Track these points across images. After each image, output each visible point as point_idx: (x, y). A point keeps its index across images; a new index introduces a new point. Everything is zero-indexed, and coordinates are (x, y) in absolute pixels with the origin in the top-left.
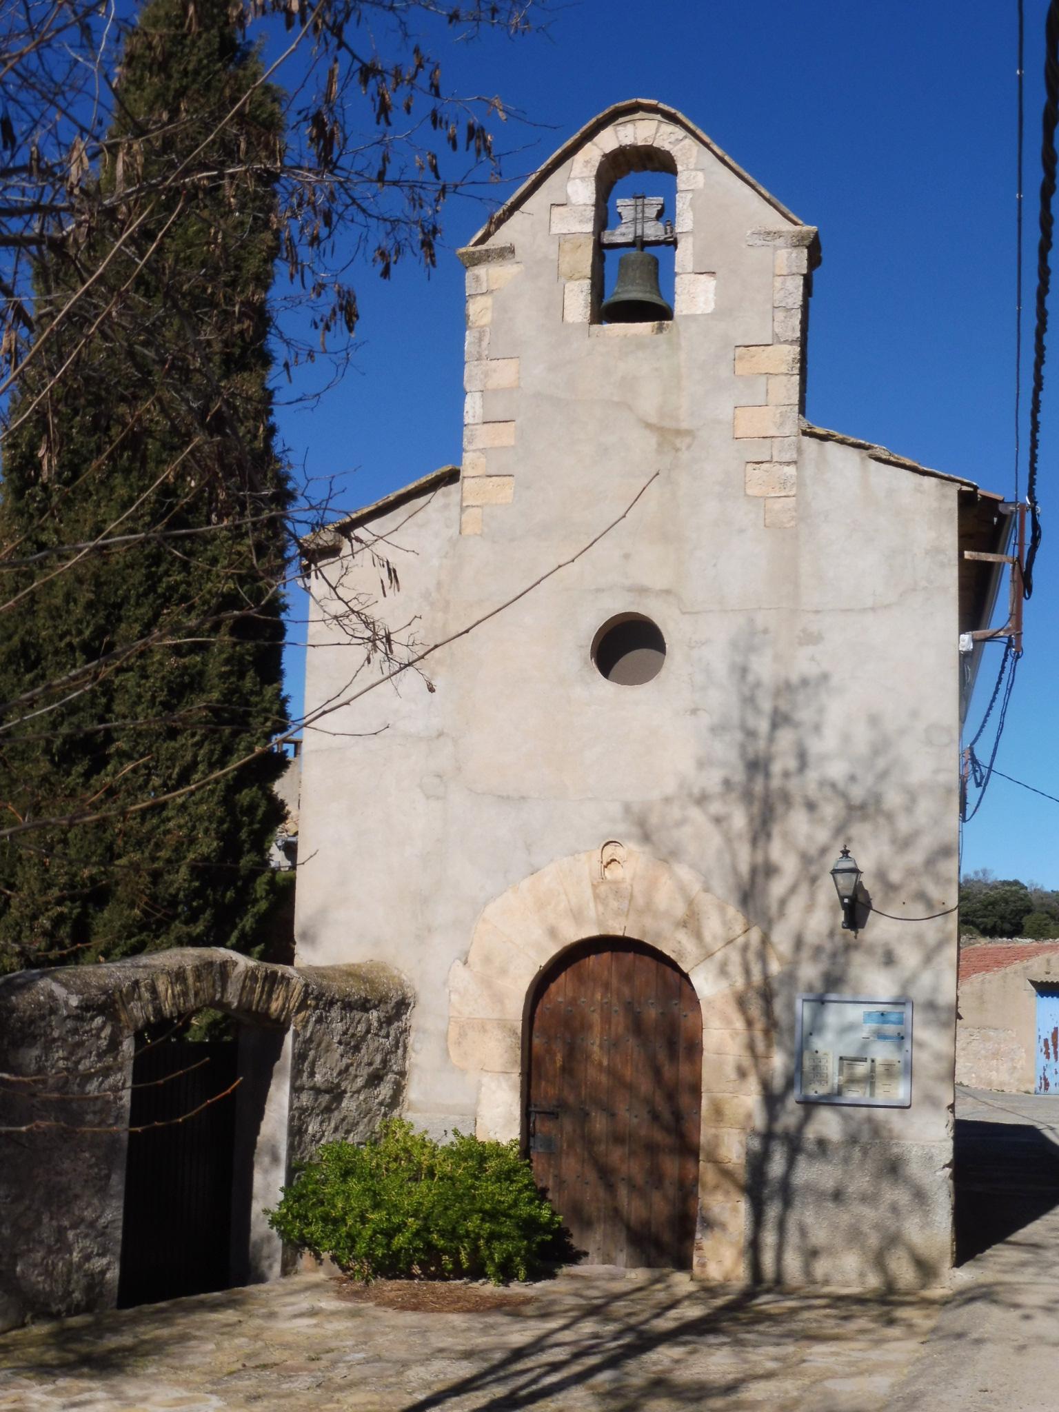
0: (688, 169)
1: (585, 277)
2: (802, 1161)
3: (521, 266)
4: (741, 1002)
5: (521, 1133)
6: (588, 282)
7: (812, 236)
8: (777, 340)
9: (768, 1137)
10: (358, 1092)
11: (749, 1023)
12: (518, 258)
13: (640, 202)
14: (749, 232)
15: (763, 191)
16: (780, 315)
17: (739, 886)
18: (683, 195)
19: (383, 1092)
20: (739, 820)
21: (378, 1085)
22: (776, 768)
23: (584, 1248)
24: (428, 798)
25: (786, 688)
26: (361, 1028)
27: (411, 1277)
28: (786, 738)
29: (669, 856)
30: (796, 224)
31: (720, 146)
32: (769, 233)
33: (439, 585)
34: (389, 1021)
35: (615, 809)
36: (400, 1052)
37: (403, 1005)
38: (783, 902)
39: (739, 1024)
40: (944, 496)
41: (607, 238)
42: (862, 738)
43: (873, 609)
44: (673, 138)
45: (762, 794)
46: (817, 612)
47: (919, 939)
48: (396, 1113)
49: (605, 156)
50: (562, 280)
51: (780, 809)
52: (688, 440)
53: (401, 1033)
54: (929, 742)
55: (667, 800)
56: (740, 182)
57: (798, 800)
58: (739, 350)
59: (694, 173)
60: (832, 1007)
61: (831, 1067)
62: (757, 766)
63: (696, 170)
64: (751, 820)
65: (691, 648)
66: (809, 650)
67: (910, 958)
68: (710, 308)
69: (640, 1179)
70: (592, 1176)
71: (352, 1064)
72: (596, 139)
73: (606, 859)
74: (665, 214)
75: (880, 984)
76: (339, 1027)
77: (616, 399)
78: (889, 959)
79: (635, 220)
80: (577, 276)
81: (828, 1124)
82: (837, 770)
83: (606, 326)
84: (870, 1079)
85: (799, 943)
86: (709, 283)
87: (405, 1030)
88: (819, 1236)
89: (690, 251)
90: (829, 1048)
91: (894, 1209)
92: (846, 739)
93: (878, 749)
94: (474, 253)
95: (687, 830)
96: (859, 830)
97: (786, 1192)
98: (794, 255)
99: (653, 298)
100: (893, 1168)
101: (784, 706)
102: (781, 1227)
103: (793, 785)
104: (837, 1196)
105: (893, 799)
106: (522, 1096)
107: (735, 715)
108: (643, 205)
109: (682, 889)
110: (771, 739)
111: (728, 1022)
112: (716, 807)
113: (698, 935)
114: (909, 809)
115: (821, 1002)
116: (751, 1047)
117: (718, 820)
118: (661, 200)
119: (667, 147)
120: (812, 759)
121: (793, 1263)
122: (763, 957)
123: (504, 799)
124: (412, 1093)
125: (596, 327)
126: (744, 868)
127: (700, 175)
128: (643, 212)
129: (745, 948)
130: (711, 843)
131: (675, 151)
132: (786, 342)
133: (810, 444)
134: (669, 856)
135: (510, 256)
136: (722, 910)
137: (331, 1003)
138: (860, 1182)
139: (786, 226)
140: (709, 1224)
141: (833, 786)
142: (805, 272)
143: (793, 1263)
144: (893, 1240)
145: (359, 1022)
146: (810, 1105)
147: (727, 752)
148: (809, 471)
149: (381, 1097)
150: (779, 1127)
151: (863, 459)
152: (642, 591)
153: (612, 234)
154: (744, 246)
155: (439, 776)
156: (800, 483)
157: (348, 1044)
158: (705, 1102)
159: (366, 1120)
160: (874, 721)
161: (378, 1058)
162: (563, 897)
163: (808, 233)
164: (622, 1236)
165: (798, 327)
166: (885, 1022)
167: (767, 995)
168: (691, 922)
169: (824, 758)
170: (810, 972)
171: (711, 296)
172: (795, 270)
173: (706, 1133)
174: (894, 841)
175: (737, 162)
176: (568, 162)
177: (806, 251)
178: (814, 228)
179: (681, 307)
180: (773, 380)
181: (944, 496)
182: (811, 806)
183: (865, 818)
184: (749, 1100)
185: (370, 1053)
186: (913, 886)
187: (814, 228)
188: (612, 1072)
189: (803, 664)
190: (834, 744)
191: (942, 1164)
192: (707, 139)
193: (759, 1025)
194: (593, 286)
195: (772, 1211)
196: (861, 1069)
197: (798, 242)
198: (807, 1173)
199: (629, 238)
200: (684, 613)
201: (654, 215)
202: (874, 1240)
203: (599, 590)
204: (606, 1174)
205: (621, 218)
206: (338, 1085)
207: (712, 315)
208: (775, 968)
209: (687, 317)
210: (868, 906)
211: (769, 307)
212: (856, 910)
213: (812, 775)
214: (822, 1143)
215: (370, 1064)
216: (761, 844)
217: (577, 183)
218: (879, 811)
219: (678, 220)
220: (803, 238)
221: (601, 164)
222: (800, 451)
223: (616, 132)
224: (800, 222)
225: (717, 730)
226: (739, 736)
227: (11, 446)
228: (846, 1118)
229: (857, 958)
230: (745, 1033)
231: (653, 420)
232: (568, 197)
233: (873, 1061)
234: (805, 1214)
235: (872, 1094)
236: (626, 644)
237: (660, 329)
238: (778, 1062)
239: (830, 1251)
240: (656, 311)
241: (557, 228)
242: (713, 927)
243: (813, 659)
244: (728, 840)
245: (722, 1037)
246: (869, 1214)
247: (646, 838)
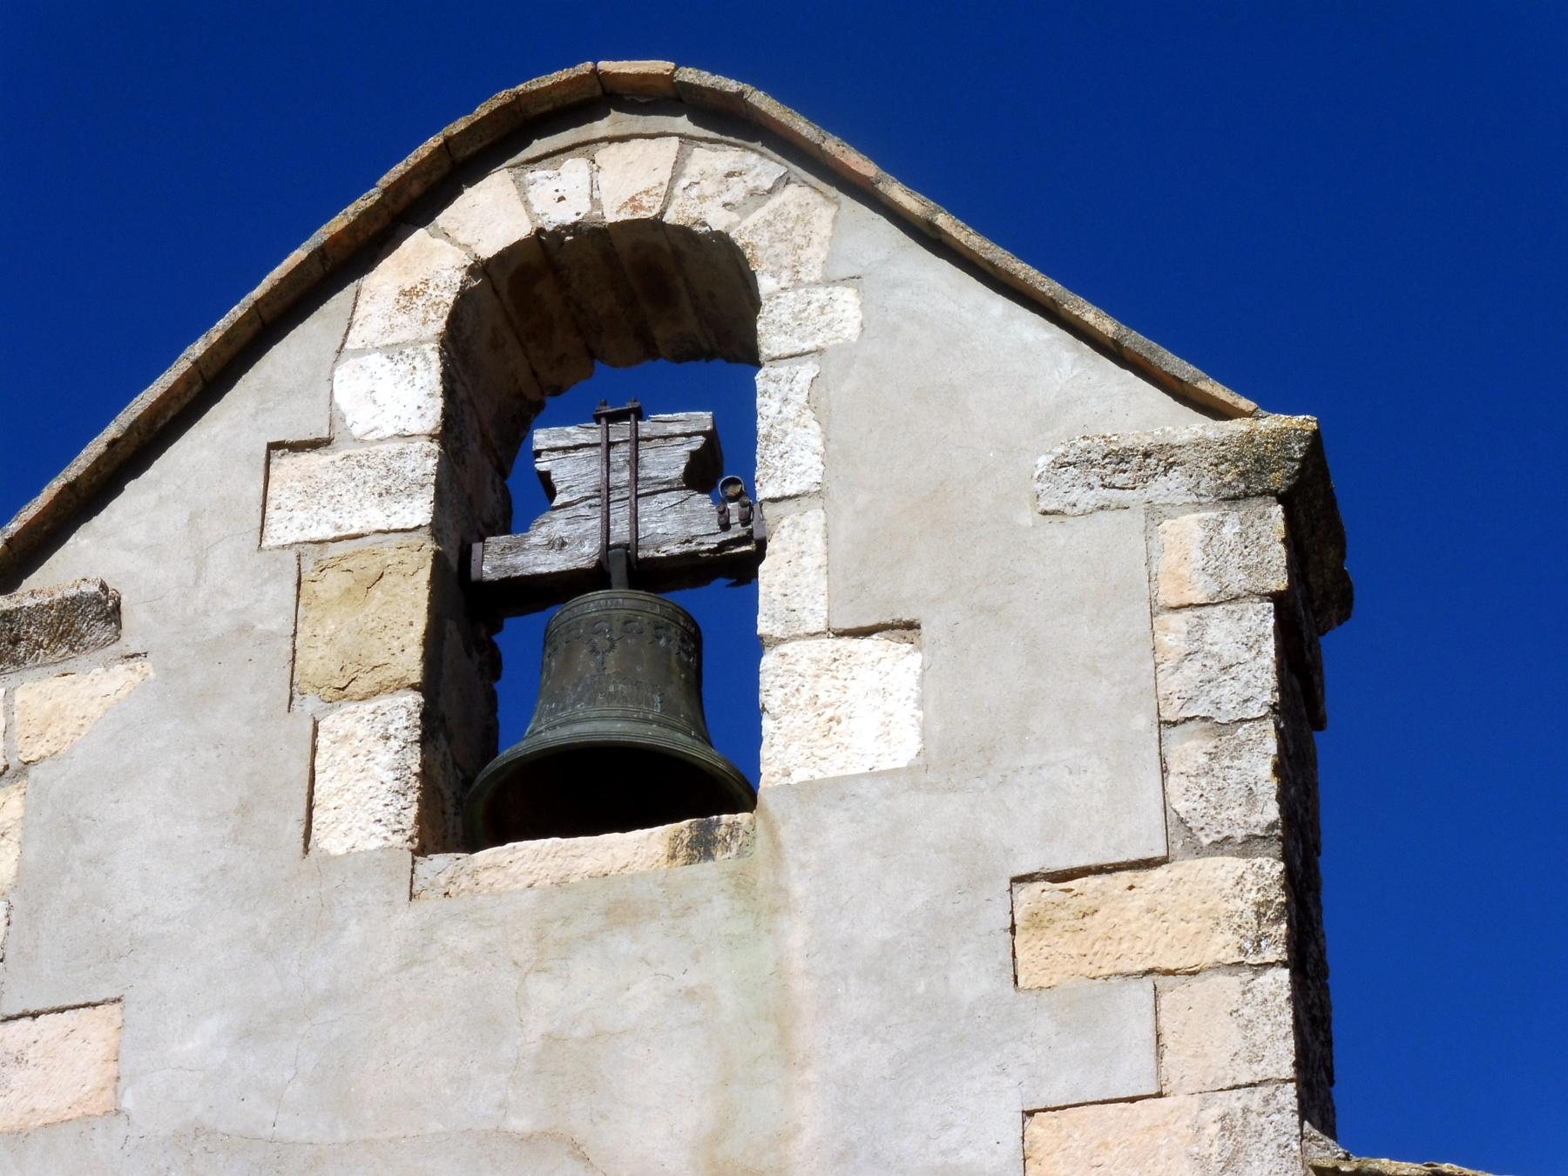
0: (797, 283)
1: (399, 685)
3: (146, 667)
6: (413, 700)
7: (1297, 450)
8: (1185, 840)
12: (131, 640)
13: (621, 431)
14: (1043, 461)
15: (1091, 315)
16: (1189, 750)
18: (782, 370)
31: (913, 182)
32: (1121, 458)
41: (496, 560)
44: (737, 190)
49: (480, 269)
50: (309, 704)
52: (1225, 492)
56: (999, 305)
58: (1029, 895)
59: (821, 294)
63: (830, 282)
68: (904, 749)
72: (444, 219)
74: (720, 468)
77: (520, 1124)
79: (605, 492)
80: (364, 684)
86: (894, 663)
89: (815, 558)
98: (1230, 530)
99: (682, 742)
108: (636, 441)
118: (703, 419)
119: (717, 219)
125: (441, 864)
127: (847, 302)
128: (635, 462)
131: (747, 230)
132: (1222, 845)
135: (101, 631)
139: (1190, 427)
142: (1279, 582)
153: (517, 548)
154: (1027, 517)
163: (1281, 440)
165: (1268, 787)
172: (1237, 581)
175: (981, 230)
176: (338, 303)
177: (1277, 511)
178: (1305, 423)
179: (784, 756)
180: (1176, 995)
187: (1305, 423)
192: (861, 165)
194: (432, 726)
197: (1241, 483)
199: (584, 554)
201: (677, 472)
205: (551, 492)
207: (912, 776)
209: (810, 791)
211: (1143, 722)
217: (372, 370)
219: (767, 456)
220: (1262, 464)
221: (465, 297)
223: (522, 188)
224: (1245, 404)
232: (334, 417)
237: (703, 847)
240: (690, 780)
241: (282, 530)
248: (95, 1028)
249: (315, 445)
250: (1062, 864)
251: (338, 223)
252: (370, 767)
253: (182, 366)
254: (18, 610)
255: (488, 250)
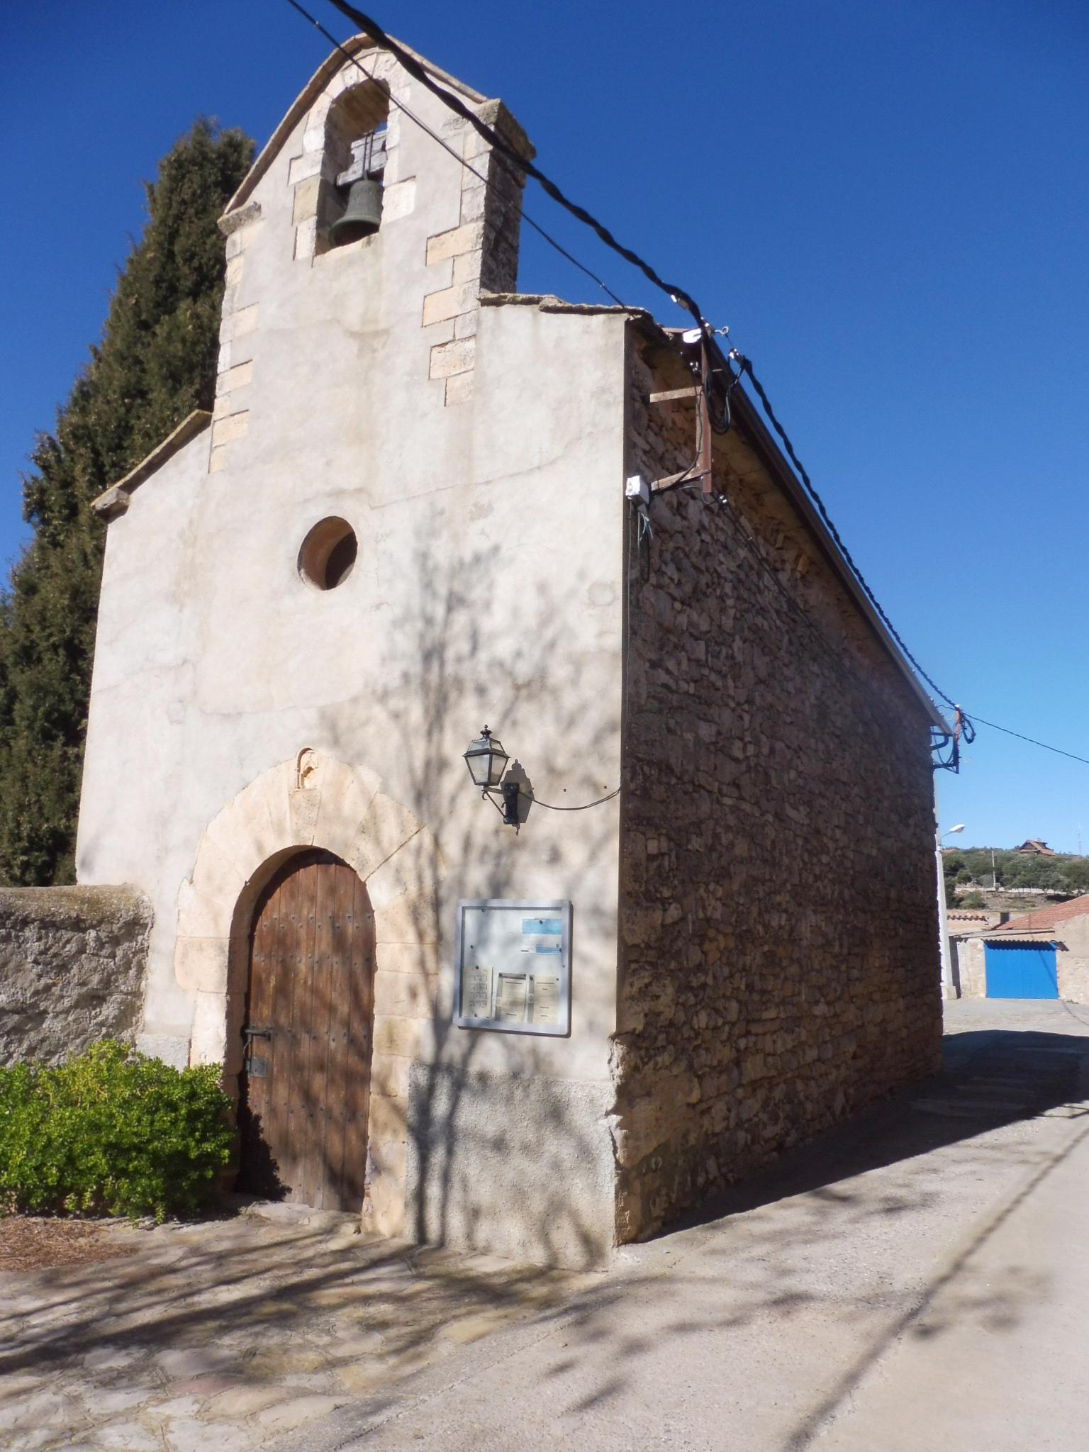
2: (465, 1099)
4: (415, 914)
5: (227, 1055)
9: (435, 1068)
10: (67, 1012)
11: (421, 936)
12: (263, 215)
17: (414, 785)
19: (105, 1013)
20: (417, 715)
21: (100, 1005)
22: (450, 654)
23: (287, 1184)
24: (172, 722)
25: (459, 568)
26: (71, 948)
27: (63, 1213)
28: (461, 619)
29: (353, 759)
30: (479, 102)
33: (191, 522)
34: (115, 941)
35: (311, 716)
36: (132, 972)
37: (136, 926)
38: (453, 799)
39: (411, 937)
40: (611, 331)
42: (531, 604)
43: (539, 468)
45: (436, 680)
46: (488, 482)
47: (585, 833)
48: (126, 1035)
51: (453, 696)
53: (135, 954)
54: (592, 603)
55: (355, 700)
57: (469, 686)
60: (497, 915)
61: (492, 984)
62: (432, 654)
64: (426, 711)
65: (377, 542)
66: (480, 524)
67: (575, 854)
69: (337, 1110)
70: (297, 1102)
71: (54, 984)
73: (303, 768)
75: (542, 886)
76: (36, 946)
77: (329, 317)
78: (555, 857)
81: (491, 1057)
82: (503, 648)
83: (328, 254)
84: (530, 1004)
85: (467, 845)
87: (142, 950)
88: (484, 1193)
90: (493, 961)
91: (556, 1165)
92: (516, 612)
93: (546, 618)
94: (228, 220)
95: (371, 729)
96: (525, 710)
97: (451, 1133)
100: (555, 1114)
101: (458, 587)
102: (446, 1179)
103: (465, 670)
104: (499, 1144)
105: (559, 672)
106: (229, 1015)
107: (416, 603)
109: (364, 791)
110: (447, 623)
111: (401, 934)
112: (395, 703)
113: (378, 842)
114: (574, 682)
115: (484, 908)
116: (422, 963)
117: (396, 716)
120: (482, 640)
121: (456, 1222)
122: (434, 863)
123: (227, 716)
124: (149, 1013)
126: (419, 764)
129: (419, 851)
130: (389, 743)
132: (472, 220)
133: (488, 311)
134: (353, 759)
135: (256, 214)
136: (399, 812)
137: (25, 922)
138: (524, 1131)
140: (378, 1169)
141: (501, 664)
143: (456, 1222)
144: (558, 1206)
145: (68, 941)
146: (476, 1032)
147: (407, 643)
148: (486, 339)
149: (100, 1019)
150: (445, 1058)
151: (535, 315)
152: (338, 494)
155: (181, 701)
156: (478, 354)
157: (46, 964)
158: (377, 1025)
159: (78, 1041)
160: (542, 588)
161: (95, 979)
162: (266, 809)
164: (321, 1172)
166: (548, 931)
167: (437, 905)
168: (370, 828)
169: (493, 636)
170: (477, 876)
171: (412, 200)
173: (378, 1062)
174: (558, 719)
175: (441, 67)
176: (305, 117)
178: (497, 101)
181: (611, 331)
182: (481, 691)
183: (530, 697)
184: (418, 1026)
185: (88, 972)
186: (580, 772)
187: (497, 101)
188: (315, 991)
189: (475, 542)
190: (505, 621)
191: (604, 1110)
193: (430, 936)
195: (438, 1157)
196: (523, 989)
198: (476, 1115)
200: (372, 509)
202: (537, 1204)
203: (306, 501)
204: (309, 1099)
206: (34, 1005)
208: (444, 872)
210: (530, 797)
212: (516, 800)
213: (483, 656)
214: (483, 1077)
215: (83, 984)
216: (435, 737)
218: (543, 687)
221: (331, 110)
222: (478, 322)
224: (484, 98)
225: (398, 624)
226: (419, 625)
227: (28, 496)
228: (509, 1048)
229: (523, 858)
230: (416, 947)
231: (356, 328)
233: (531, 978)
234: (470, 1163)
235: (530, 1020)
236: (330, 554)
238: (447, 980)
239: (494, 1214)
242: (390, 831)
243: (483, 532)
244: (406, 735)
245: (396, 953)
246: (535, 1171)
247: (336, 741)
248: (254, 310)
249: (299, 157)
250: (438, 232)
251: (300, 96)
252: (307, 233)
253: (270, 142)
254: (736, 377)
255: (335, 96)
